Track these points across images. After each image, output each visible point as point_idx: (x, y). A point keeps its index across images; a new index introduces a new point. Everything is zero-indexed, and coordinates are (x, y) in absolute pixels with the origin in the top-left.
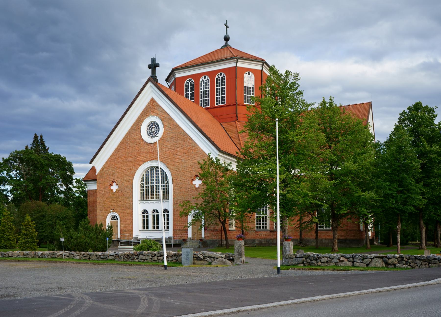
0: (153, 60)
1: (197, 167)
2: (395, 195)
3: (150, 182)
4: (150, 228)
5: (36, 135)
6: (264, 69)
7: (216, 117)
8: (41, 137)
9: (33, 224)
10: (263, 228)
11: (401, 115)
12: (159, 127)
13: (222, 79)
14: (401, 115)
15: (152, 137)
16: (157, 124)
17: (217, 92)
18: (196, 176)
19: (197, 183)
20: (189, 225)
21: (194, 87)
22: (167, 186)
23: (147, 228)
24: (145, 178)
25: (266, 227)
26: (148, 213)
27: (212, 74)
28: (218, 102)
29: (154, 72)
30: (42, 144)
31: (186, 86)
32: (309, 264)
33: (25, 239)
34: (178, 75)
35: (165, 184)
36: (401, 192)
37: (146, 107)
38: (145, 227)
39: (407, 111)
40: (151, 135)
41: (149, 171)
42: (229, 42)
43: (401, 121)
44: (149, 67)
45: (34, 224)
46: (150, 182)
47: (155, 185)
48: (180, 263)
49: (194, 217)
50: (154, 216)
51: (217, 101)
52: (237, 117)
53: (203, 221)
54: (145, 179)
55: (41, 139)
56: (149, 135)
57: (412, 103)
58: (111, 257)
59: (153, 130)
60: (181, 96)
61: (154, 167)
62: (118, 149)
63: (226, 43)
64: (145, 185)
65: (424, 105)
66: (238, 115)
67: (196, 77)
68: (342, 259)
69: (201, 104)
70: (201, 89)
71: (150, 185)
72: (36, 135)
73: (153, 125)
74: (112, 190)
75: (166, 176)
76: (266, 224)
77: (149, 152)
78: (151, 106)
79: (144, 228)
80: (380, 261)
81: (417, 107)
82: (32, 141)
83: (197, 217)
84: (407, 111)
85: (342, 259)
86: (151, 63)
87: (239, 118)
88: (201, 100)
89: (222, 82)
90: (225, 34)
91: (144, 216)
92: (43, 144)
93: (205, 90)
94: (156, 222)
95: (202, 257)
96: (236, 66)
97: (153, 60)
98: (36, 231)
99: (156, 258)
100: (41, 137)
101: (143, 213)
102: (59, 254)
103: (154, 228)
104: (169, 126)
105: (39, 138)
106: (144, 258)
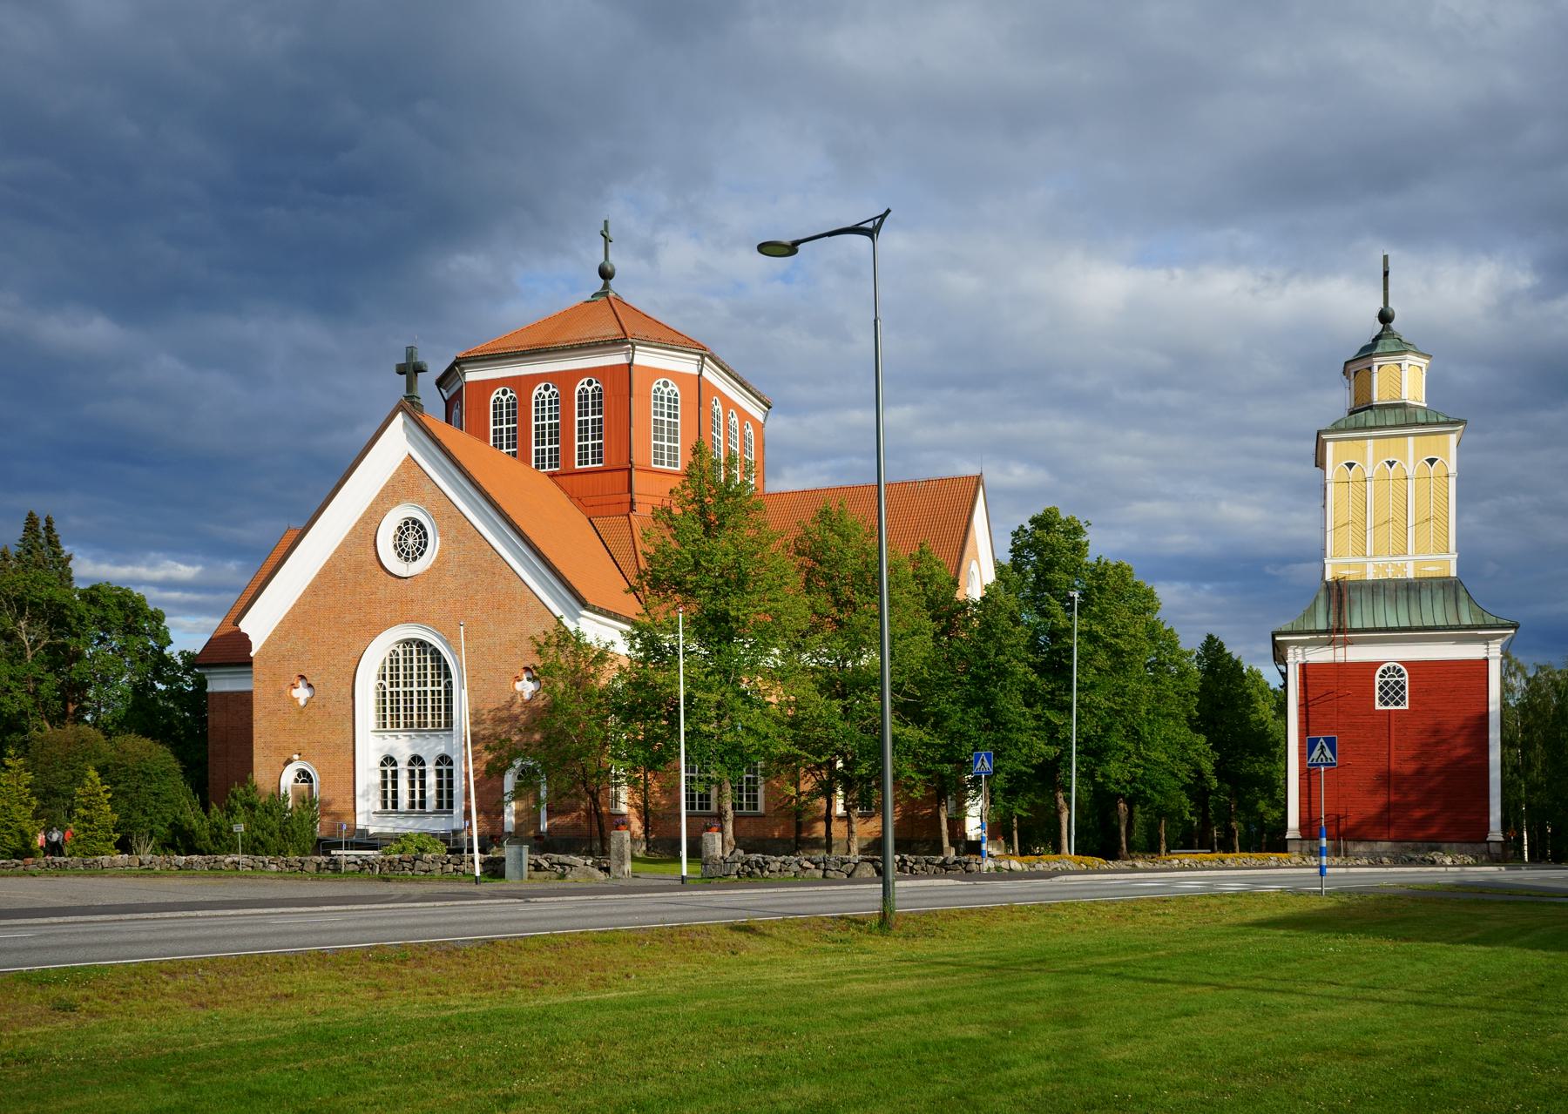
0: (410, 352)
1: (529, 646)
2: (973, 733)
3: (401, 679)
4: (431, 804)
5: (31, 514)
6: (706, 373)
7: (578, 499)
8: (49, 521)
9: (103, 791)
10: (701, 807)
11: (1015, 534)
12: (425, 535)
13: (593, 397)
14: (1015, 534)
15: (407, 559)
16: (422, 526)
17: (580, 431)
18: (527, 669)
19: (526, 688)
20: (506, 798)
21: (516, 411)
22: (447, 693)
23: (395, 805)
24: (391, 672)
25: (708, 807)
26: (395, 764)
27: (565, 380)
28: (583, 458)
29: (410, 386)
30: (50, 542)
31: (495, 407)
32: (749, 875)
33: (85, 830)
34: (473, 375)
35: (442, 688)
36: (987, 728)
37: (392, 478)
38: (389, 802)
39: (1028, 527)
40: (405, 554)
41: (400, 651)
42: (611, 282)
43: (1016, 551)
44: (401, 370)
45: (107, 792)
46: (401, 679)
47: (415, 688)
48: (502, 876)
49: (519, 777)
50: (412, 773)
51: (580, 456)
52: (632, 502)
53: (544, 788)
54: (388, 673)
55: (49, 528)
56: (399, 555)
57: (1038, 511)
58: (351, 867)
59: (410, 541)
60: (483, 445)
61: (414, 640)
62: (314, 590)
63: (606, 286)
64: (388, 689)
65: (1063, 517)
66: (637, 498)
67: (522, 385)
68: (806, 864)
69: (537, 460)
70: (537, 419)
71: (401, 689)
72: (31, 514)
73: (412, 526)
74: (295, 700)
75: (446, 666)
76: (755, 798)
77: (403, 600)
78: (404, 476)
79: (385, 805)
80: (869, 866)
81: (1043, 522)
82: (20, 534)
83: (526, 776)
84: (1028, 527)
85: (806, 864)
86: (404, 361)
87: (636, 507)
88: (537, 452)
89: (593, 405)
90: (602, 259)
91: (384, 773)
92: (52, 542)
93: (547, 422)
94: (445, 789)
95: (546, 865)
96: (630, 365)
97: (410, 352)
98: (113, 811)
99: (451, 868)
100: (49, 521)
101: (382, 764)
102: (228, 860)
103: (440, 805)
104: (453, 533)
105: (43, 524)
106: (425, 867)
